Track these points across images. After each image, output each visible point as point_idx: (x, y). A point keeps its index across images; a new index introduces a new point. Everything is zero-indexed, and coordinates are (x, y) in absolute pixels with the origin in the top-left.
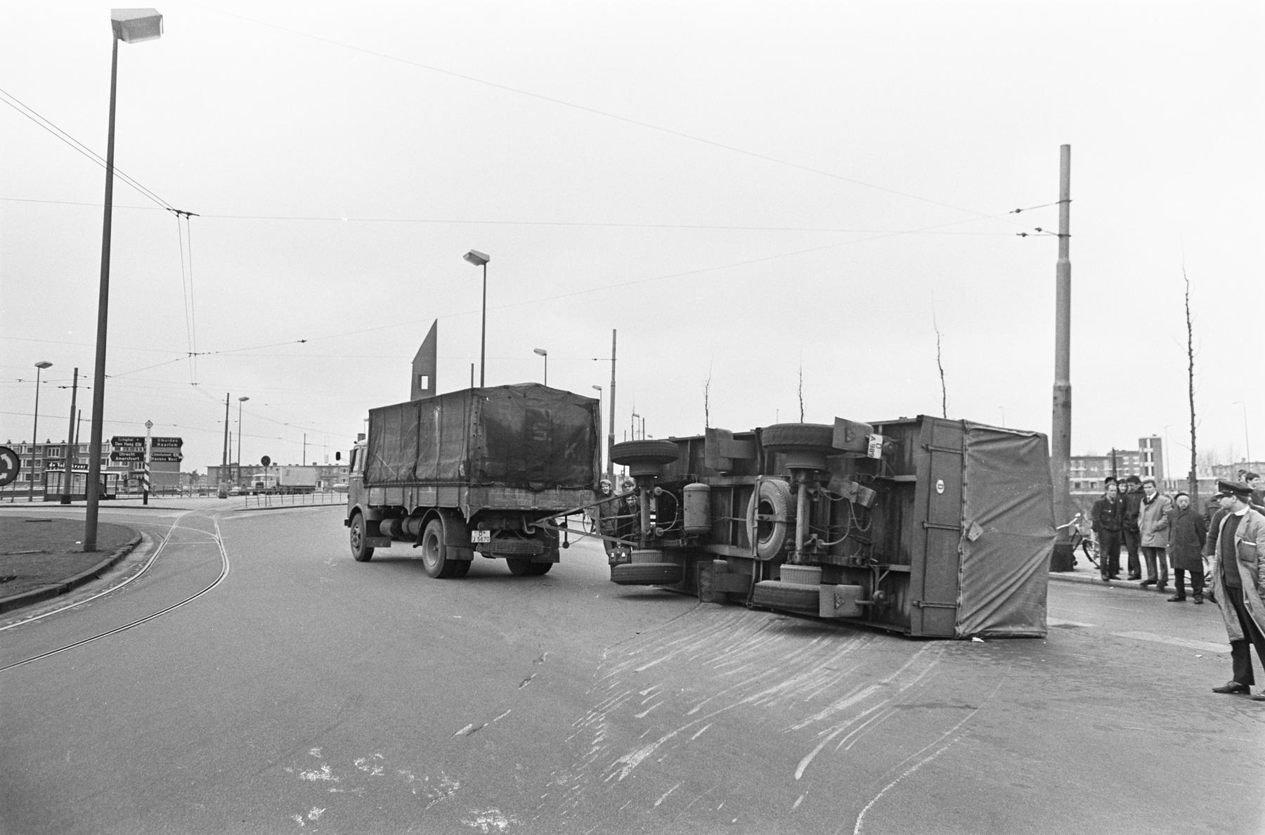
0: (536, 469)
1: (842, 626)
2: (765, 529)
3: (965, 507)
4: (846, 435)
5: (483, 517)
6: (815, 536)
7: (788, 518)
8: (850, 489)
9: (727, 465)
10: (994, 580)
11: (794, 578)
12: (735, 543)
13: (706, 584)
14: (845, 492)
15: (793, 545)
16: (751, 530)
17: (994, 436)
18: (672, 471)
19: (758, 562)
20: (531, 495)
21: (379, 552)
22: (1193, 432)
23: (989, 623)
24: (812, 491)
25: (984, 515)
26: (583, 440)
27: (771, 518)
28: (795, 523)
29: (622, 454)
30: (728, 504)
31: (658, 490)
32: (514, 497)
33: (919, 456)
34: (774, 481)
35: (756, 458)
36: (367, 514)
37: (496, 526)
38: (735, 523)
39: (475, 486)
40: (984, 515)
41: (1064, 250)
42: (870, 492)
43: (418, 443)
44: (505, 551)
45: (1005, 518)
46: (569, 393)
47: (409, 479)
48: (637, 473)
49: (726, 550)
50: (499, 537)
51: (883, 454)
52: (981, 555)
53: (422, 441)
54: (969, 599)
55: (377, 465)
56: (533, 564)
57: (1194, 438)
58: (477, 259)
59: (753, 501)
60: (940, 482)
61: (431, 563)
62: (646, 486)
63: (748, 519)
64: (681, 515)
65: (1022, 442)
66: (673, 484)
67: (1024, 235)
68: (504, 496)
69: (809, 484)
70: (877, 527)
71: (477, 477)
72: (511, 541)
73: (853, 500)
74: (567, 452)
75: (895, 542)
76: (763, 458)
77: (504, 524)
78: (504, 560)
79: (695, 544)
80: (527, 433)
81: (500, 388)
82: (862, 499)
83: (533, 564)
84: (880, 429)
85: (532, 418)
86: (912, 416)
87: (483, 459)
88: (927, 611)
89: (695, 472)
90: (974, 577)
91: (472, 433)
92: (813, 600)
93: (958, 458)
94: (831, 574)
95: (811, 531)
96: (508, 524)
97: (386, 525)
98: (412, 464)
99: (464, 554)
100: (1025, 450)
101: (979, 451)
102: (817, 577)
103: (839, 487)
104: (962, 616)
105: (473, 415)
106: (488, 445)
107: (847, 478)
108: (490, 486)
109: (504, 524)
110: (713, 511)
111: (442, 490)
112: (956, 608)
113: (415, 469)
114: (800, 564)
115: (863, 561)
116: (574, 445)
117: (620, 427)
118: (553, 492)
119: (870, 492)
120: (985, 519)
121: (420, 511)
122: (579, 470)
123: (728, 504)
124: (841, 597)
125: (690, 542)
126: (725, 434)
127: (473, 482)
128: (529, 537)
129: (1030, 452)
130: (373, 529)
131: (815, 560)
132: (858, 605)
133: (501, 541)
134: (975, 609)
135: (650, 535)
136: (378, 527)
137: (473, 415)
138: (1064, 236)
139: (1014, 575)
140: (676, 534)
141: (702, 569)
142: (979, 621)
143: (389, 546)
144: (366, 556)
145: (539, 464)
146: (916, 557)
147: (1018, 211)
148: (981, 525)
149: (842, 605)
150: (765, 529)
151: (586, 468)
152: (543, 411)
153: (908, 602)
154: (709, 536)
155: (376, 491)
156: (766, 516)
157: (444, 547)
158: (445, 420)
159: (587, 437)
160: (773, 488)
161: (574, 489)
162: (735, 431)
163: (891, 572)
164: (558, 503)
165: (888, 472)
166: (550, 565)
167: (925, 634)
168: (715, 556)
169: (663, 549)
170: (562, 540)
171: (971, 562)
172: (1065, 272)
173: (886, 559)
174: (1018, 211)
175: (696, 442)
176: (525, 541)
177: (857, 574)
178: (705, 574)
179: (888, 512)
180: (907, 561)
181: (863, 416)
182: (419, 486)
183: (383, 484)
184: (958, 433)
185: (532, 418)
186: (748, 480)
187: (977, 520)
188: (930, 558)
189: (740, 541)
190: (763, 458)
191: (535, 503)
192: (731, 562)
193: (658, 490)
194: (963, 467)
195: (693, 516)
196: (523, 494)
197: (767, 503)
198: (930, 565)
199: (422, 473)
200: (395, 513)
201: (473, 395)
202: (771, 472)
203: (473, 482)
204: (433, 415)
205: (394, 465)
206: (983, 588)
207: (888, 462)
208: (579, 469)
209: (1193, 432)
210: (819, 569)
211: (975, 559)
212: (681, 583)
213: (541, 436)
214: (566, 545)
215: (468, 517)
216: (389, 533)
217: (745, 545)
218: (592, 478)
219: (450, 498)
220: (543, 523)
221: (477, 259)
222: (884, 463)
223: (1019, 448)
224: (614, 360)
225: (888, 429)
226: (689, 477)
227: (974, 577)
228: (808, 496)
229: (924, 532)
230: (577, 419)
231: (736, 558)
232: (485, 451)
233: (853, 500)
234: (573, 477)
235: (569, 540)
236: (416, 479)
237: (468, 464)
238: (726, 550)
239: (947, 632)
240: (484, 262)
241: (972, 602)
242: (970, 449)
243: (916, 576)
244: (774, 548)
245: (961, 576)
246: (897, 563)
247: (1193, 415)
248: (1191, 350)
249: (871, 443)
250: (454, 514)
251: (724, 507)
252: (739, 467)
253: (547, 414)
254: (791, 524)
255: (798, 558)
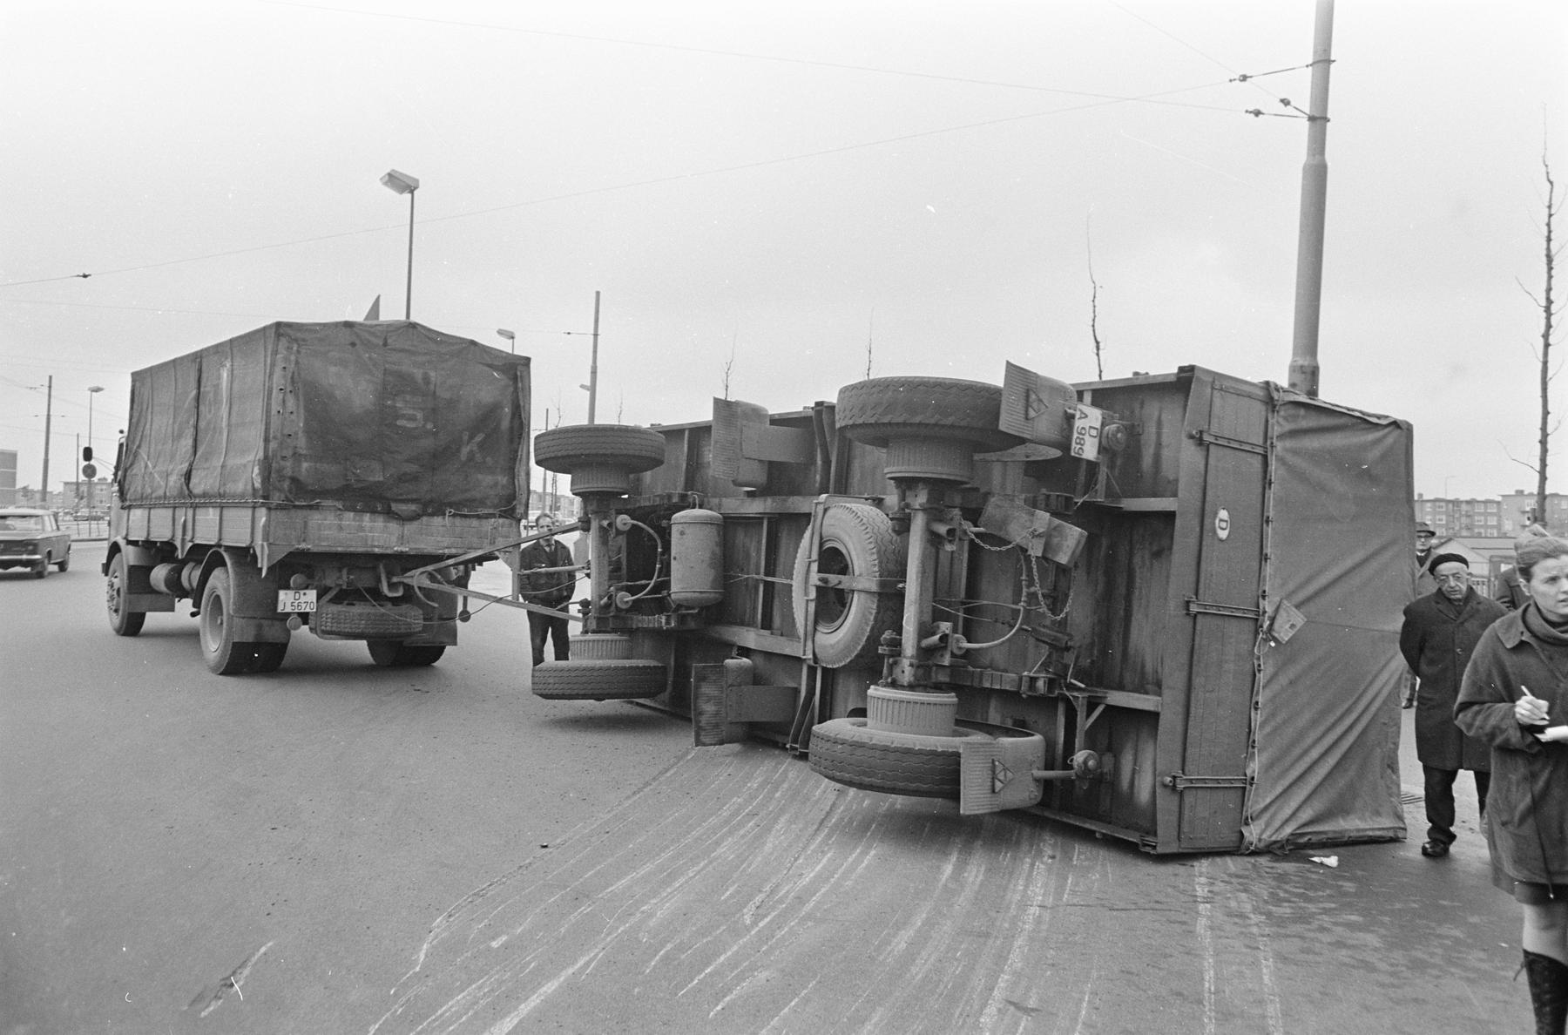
0: (402, 478)
1: (1007, 828)
2: (831, 604)
3: (1269, 569)
4: (1027, 405)
5: (298, 566)
6: (945, 627)
7: (882, 584)
8: (1030, 527)
9: (761, 478)
10: (1314, 723)
11: (894, 719)
12: (767, 624)
13: (709, 708)
14: (1018, 533)
15: (896, 644)
16: (802, 605)
17: (1325, 421)
18: (658, 483)
19: (812, 671)
20: (394, 526)
21: (153, 620)
22: (1543, 442)
23: (1306, 815)
24: (942, 529)
25: (1301, 586)
26: (497, 428)
27: (845, 582)
28: (901, 595)
29: (570, 451)
30: (755, 547)
31: (623, 521)
32: (361, 529)
33: (1183, 459)
34: (854, 506)
35: (813, 461)
36: (130, 555)
37: (329, 582)
38: (769, 587)
39: (279, 507)
40: (1301, 586)
41: (1318, 144)
42: (1073, 535)
43: (196, 427)
44: (362, 626)
45: (1337, 592)
46: (473, 343)
47: (181, 495)
48: (583, 487)
49: (751, 638)
50: (337, 600)
51: (1102, 449)
52: (1292, 672)
53: (202, 424)
54: (1270, 766)
55: (138, 469)
56: (409, 655)
57: (1544, 451)
58: (402, 184)
59: (805, 550)
60: (1223, 514)
61: (213, 647)
62: (602, 513)
63: (797, 583)
64: (666, 570)
65: (1372, 436)
66: (654, 509)
67: (1258, 113)
68: (340, 528)
69: (935, 512)
70: (1079, 611)
71: (285, 490)
72: (358, 609)
73: (1036, 550)
74: (465, 450)
75: (1116, 639)
76: (827, 462)
77: (343, 579)
78: (365, 642)
79: (692, 625)
80: (384, 416)
81: (337, 324)
82: (1059, 548)
83: (409, 655)
84: (1088, 397)
85: (396, 385)
86: (1164, 366)
87: (297, 456)
88: (1189, 799)
89: (695, 488)
90: (1279, 719)
91: (275, 408)
92: (943, 777)
93: (1257, 462)
94: (971, 697)
95: (938, 616)
96: (352, 578)
97: (159, 574)
98: (185, 466)
99: (272, 633)
100: (1375, 453)
101: (1295, 452)
102: (949, 715)
103: (1004, 523)
104: (1255, 803)
105: (278, 372)
106: (309, 432)
107: (1019, 502)
108: (310, 507)
109: (343, 579)
110: (726, 562)
111: (228, 513)
112: (1243, 789)
113: (188, 476)
114: (911, 687)
115: (1051, 683)
116: (479, 438)
117: (554, 406)
118: (437, 520)
119: (1073, 535)
120: (1301, 596)
121: (198, 551)
122: (489, 482)
123: (755, 547)
124: (1003, 765)
125: (682, 619)
126: (755, 413)
127: (276, 499)
128: (395, 601)
129: (1383, 457)
130: (138, 577)
131: (943, 678)
132: (1037, 780)
133: (334, 608)
134: (1279, 789)
135: (608, 606)
136: (153, 575)
137: (278, 372)
138: (1318, 120)
139: (1349, 711)
140: (661, 605)
141: (702, 678)
142: (1288, 812)
143: (172, 609)
144: (132, 626)
145: (412, 468)
146: (1174, 679)
147: (1244, 78)
148: (1298, 607)
149: (1006, 784)
150: (831, 604)
151: (503, 480)
152: (418, 374)
153: (1144, 773)
154: (721, 608)
155: (138, 515)
156: (833, 579)
157: (230, 617)
158: (236, 386)
159: (505, 424)
160: (853, 523)
161: (479, 517)
162: (775, 408)
163: (1112, 710)
164: (446, 541)
165: (1109, 493)
166: (441, 650)
167: (1185, 847)
168: (728, 648)
169: (631, 632)
170: (460, 609)
171: (1275, 687)
172: (1317, 177)
173: (1099, 676)
174: (1244, 78)
175: (699, 433)
176: (386, 610)
177: (1024, 709)
178: (707, 689)
179: (1101, 579)
180: (1158, 687)
181: (1068, 363)
182: (195, 507)
183: (148, 503)
184: (1259, 409)
185: (396, 385)
186: (799, 504)
187: (1289, 596)
188: (1198, 681)
189: (777, 621)
190: (827, 462)
191: (401, 539)
192: (760, 660)
193: (623, 521)
194: (1266, 483)
195: (689, 571)
196: (380, 522)
197: (836, 553)
198: (1198, 695)
199: (199, 484)
200: (158, 551)
201: (278, 335)
202: (843, 488)
203: (276, 499)
204: (219, 377)
205: (160, 472)
206: (1293, 743)
207: (1111, 467)
208: (488, 479)
209: (1543, 442)
210: (951, 698)
211: (1283, 680)
212: (665, 696)
213: (412, 418)
214: (466, 616)
215: (264, 564)
216: (163, 588)
217: (789, 631)
218: (512, 497)
219: (239, 528)
220: (418, 578)
221: (402, 184)
222: (1103, 471)
223: (1364, 447)
224: (596, 335)
225: (1104, 395)
226: (683, 497)
227: (1279, 719)
228: (934, 540)
229: (1188, 622)
230: (488, 390)
231: (769, 655)
232: (302, 442)
233: (1036, 550)
234: (477, 494)
235: (469, 609)
236: (191, 494)
237: (267, 466)
238: (751, 638)
239: (1229, 839)
240: (412, 192)
241: (1276, 770)
242: (1279, 445)
243: (1170, 720)
244: (848, 648)
245: (1257, 718)
246: (1121, 687)
247: (1546, 413)
248: (1549, 301)
249: (1078, 424)
250: (244, 556)
251: (748, 556)
252: (778, 480)
253: (427, 380)
254: (890, 598)
255: (906, 672)
